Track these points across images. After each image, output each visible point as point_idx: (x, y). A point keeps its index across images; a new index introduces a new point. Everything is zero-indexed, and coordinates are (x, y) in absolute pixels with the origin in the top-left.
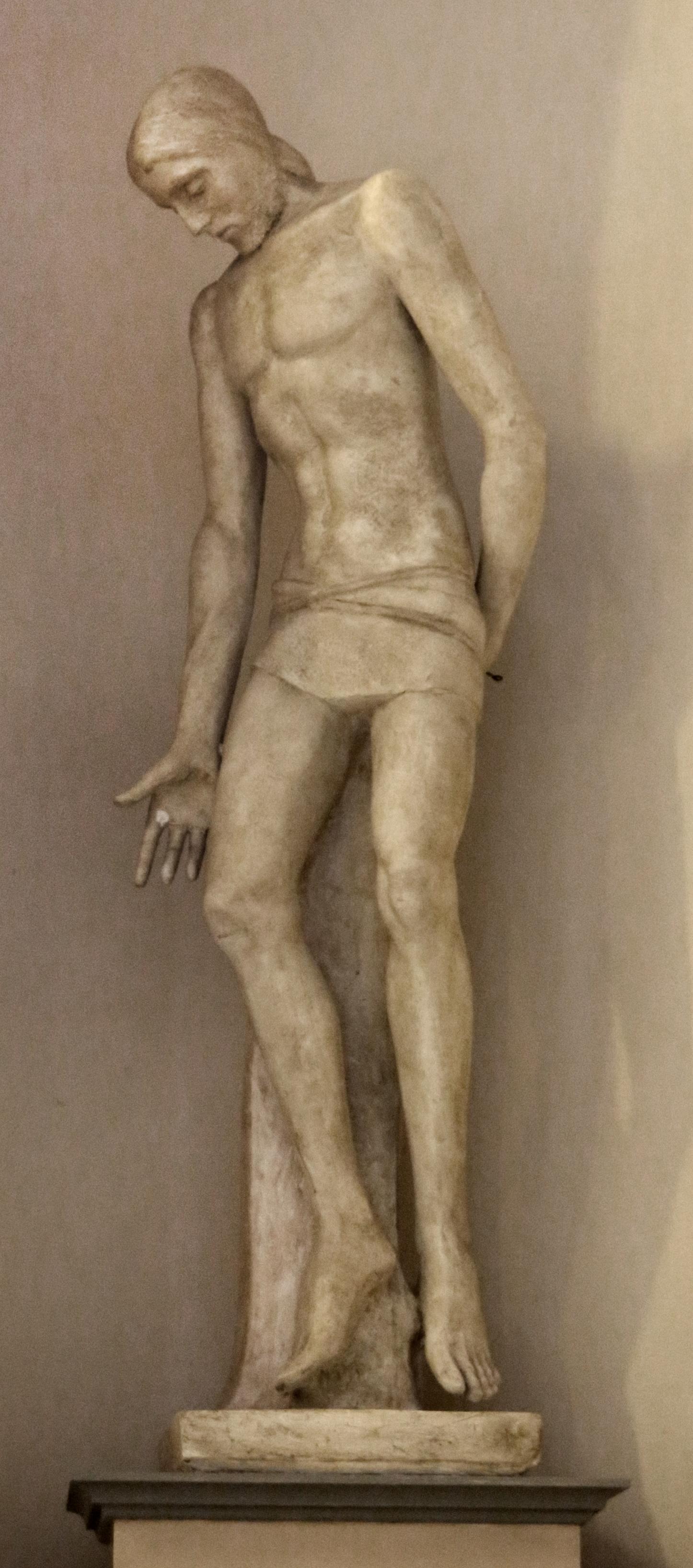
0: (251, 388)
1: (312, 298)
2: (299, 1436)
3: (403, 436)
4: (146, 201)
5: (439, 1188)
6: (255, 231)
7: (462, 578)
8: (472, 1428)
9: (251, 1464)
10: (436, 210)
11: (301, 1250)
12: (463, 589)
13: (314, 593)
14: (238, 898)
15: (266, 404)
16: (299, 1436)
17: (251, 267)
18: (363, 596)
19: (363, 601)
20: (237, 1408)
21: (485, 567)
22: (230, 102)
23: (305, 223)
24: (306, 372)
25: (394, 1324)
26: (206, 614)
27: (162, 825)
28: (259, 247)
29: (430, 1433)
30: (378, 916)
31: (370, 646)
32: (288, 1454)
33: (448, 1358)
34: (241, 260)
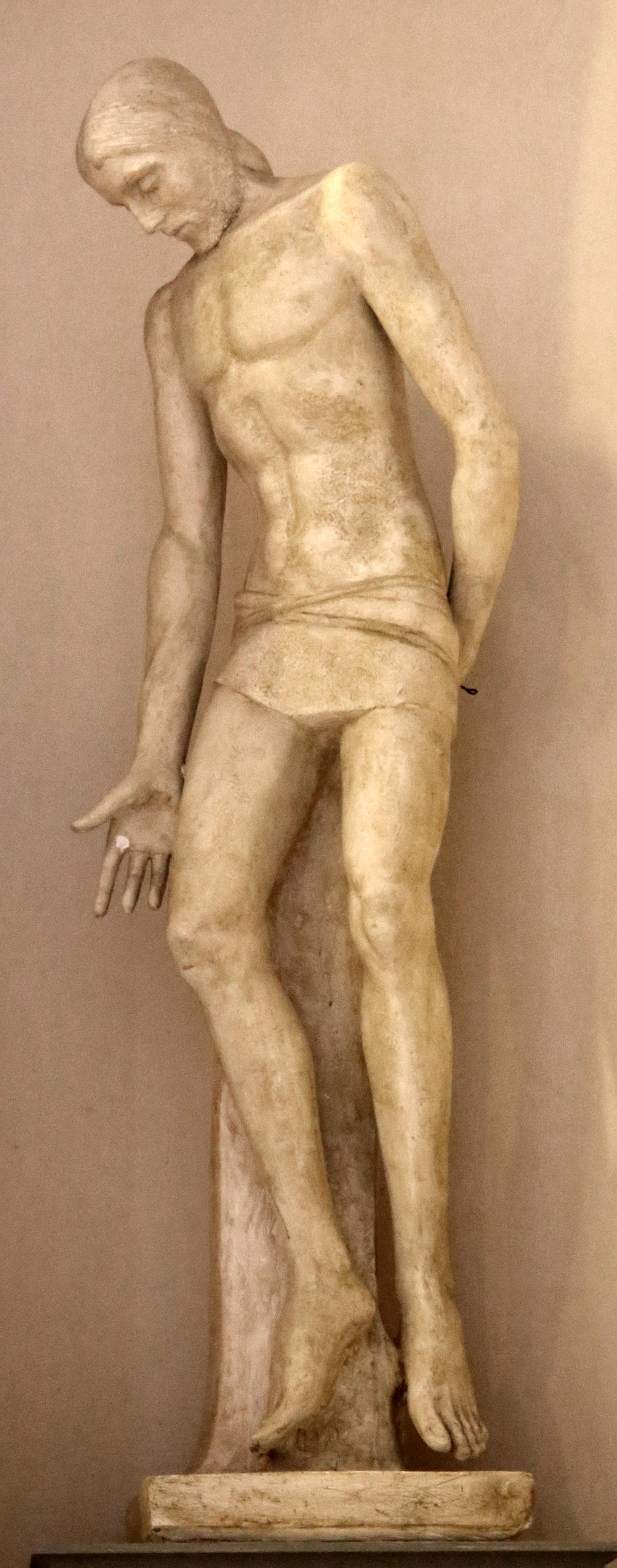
0: (209, 390)
1: (272, 298)
2: (276, 1501)
3: (368, 441)
4: (100, 202)
5: (420, 1230)
6: (212, 229)
7: (433, 587)
8: (459, 1489)
9: (225, 1533)
10: (399, 203)
11: (274, 1297)
12: (435, 598)
13: (279, 605)
14: (204, 926)
15: (223, 408)
16: (276, 1501)
17: (206, 265)
18: (330, 608)
19: (331, 613)
20: (210, 1471)
21: (458, 579)
22: (180, 88)
23: (263, 220)
24: (266, 375)
25: (374, 1378)
26: (164, 630)
27: (122, 851)
28: (216, 246)
29: (416, 1495)
30: (351, 943)
31: (339, 659)
32: (263, 1520)
33: (432, 1412)
34: (196, 259)
